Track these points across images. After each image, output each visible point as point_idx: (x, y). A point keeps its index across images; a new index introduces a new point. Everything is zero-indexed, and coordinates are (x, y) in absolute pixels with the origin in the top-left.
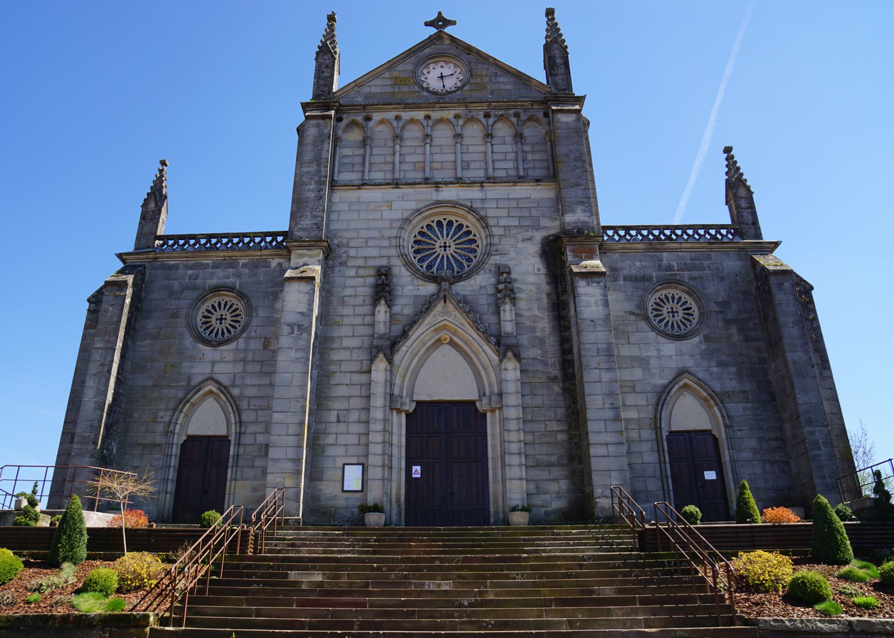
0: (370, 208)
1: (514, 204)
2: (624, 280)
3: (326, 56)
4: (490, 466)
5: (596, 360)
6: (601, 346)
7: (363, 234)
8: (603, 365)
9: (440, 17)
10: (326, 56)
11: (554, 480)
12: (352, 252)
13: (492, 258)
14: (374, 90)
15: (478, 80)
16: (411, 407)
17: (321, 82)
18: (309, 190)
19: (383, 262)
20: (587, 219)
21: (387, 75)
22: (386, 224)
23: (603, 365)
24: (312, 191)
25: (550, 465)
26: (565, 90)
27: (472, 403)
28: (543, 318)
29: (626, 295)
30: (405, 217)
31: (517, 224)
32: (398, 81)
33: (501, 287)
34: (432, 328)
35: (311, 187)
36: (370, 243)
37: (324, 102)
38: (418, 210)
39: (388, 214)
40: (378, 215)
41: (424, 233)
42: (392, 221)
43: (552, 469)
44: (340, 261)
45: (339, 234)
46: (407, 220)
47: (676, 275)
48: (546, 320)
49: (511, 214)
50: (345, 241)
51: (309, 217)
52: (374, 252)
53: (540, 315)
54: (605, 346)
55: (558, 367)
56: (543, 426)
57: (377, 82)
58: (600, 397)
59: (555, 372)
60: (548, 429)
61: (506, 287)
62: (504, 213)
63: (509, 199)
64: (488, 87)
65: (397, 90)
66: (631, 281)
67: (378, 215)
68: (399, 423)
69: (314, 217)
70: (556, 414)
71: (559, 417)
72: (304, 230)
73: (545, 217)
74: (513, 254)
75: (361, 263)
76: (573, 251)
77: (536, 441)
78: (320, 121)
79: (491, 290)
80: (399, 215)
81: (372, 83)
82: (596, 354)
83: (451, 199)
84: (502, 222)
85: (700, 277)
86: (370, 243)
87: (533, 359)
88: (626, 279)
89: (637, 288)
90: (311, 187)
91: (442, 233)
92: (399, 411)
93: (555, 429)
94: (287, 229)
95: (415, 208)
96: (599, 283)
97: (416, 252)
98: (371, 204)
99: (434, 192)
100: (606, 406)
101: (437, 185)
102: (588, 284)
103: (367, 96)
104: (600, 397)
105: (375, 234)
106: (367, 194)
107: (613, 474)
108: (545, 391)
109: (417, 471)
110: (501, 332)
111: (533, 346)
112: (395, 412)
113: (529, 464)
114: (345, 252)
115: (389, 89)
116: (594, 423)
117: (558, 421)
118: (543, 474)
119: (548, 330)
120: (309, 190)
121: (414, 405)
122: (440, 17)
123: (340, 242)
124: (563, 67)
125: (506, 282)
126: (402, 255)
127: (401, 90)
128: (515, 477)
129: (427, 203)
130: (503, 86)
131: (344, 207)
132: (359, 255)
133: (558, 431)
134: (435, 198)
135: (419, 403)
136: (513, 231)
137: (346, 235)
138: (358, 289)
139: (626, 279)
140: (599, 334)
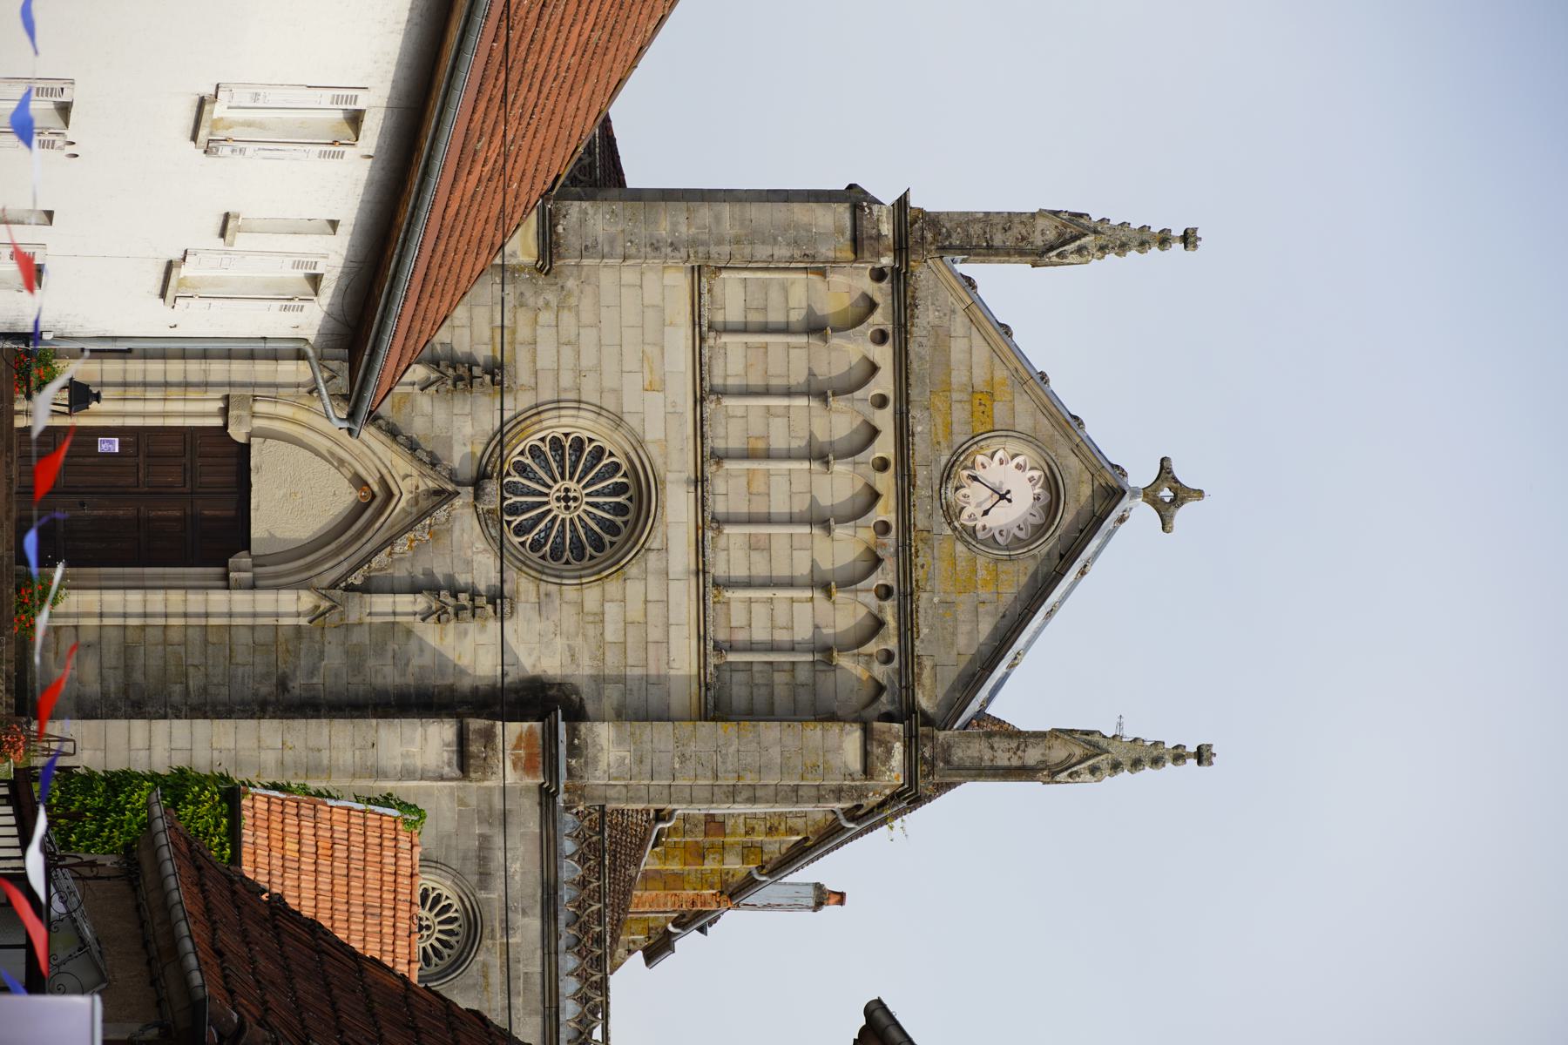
0: (648, 349)
1: (655, 634)
2: (481, 835)
3: (1062, 238)
4: (96, 570)
5: (299, 744)
6: (325, 755)
7: (589, 336)
8: (289, 756)
9: (1182, 494)
10: (1062, 238)
11: (101, 674)
12: (546, 317)
13: (532, 587)
14: (958, 348)
15: (982, 573)
16: (238, 433)
17: (975, 230)
18: (675, 225)
19: (524, 376)
20: (603, 765)
21: (1001, 373)
22: (609, 382)
23: (289, 756)
24: (674, 231)
25: (128, 669)
26: (947, 762)
27: (246, 544)
28: (403, 674)
29: (449, 836)
30: (626, 418)
31: (609, 637)
32: (982, 398)
33: (464, 598)
34: (384, 471)
35: (683, 229)
36: (567, 352)
37: (907, 245)
38: (641, 443)
39: (632, 385)
40: (631, 362)
41: (582, 450)
42: (617, 392)
43: (120, 672)
44: (528, 294)
45: (588, 289)
46: (618, 421)
47: (493, 938)
48: (398, 680)
49: (630, 628)
50: (573, 301)
51: (613, 230)
52: (546, 358)
53: (410, 669)
54: (325, 762)
55: (304, 694)
56: (196, 662)
57: (981, 352)
58: (232, 746)
59: (297, 685)
60: (191, 670)
61: (464, 608)
62: (635, 613)
63: (668, 625)
64: (963, 597)
65: (956, 396)
66: (481, 848)
67: (631, 362)
68: (199, 412)
69: (612, 241)
70: (218, 685)
71: (212, 690)
72: (582, 222)
73: (624, 695)
74: (538, 626)
75: (524, 333)
76: (531, 732)
77: (169, 648)
78: (848, 234)
79: (463, 579)
80: (630, 404)
81: (977, 340)
82: (310, 744)
83: (669, 510)
84: (612, 610)
85: (488, 985)
86: (567, 352)
87: (322, 652)
88: (485, 839)
89: (464, 859)
90: (683, 229)
91: (597, 493)
92: (225, 412)
93: (191, 684)
94: (630, 185)
95: (649, 437)
96: (449, 764)
97: (535, 452)
98: (656, 351)
99: (684, 476)
100: (216, 753)
101: (700, 481)
102: (448, 745)
103: (941, 337)
104: (232, 746)
105: (588, 360)
106: (680, 339)
107: (100, 754)
108: (260, 669)
109: (111, 445)
110: (773, 704)
111: (347, 653)
112: (221, 404)
113: (129, 633)
114: (547, 304)
115: (958, 377)
116: (187, 731)
117: (205, 689)
118: (111, 658)
119: (379, 681)
120: (675, 225)
121: (242, 439)
122: (1182, 494)
123: (570, 294)
124: (1015, 762)
125: (474, 608)
126: (537, 410)
127: (956, 406)
128: (89, 606)
129: (658, 462)
130: (964, 628)
131: (652, 292)
132: (540, 331)
133: (187, 687)
134: (670, 477)
135: (245, 449)
136: (591, 631)
137: (587, 304)
138: (467, 332)
139: (485, 839)
140: (349, 755)
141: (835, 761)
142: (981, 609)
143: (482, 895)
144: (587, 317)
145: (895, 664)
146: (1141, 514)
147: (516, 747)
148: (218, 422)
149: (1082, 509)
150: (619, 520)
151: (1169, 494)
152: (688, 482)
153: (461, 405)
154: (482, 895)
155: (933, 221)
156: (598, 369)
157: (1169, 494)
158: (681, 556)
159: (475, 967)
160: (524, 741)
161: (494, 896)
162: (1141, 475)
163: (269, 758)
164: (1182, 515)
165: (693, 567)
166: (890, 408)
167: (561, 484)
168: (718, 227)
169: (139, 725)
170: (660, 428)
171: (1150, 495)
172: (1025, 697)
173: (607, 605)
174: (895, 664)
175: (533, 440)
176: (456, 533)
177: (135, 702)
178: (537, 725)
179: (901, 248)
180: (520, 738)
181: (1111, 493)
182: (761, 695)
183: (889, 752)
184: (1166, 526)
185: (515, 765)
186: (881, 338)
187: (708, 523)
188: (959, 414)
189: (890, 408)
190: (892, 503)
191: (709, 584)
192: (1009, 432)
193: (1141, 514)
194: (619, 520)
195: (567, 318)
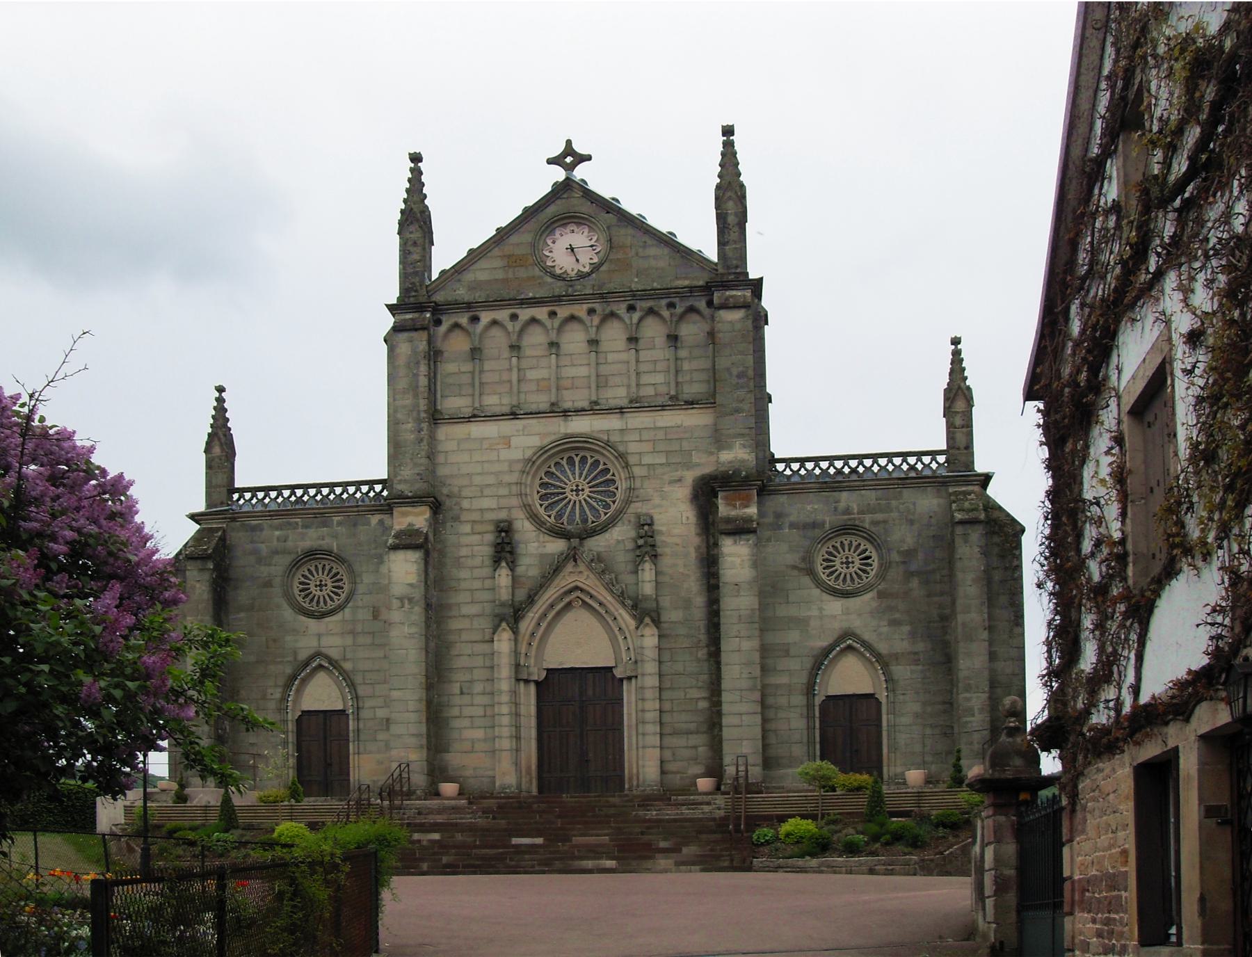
0: (485, 446)
1: (661, 435)
3: (415, 222)
6: (742, 613)
7: (478, 480)
9: (569, 149)
10: (415, 222)
14: (483, 277)
15: (620, 256)
19: (503, 515)
22: (505, 467)
27: (610, 669)
31: (664, 461)
32: (513, 261)
36: (486, 492)
39: (505, 454)
41: (547, 484)
42: (511, 462)
57: (483, 264)
62: (646, 447)
65: (510, 275)
66: (798, 528)
68: (529, 697)
71: (700, 684)
75: (476, 516)
76: (726, 498)
84: (647, 460)
92: (527, 681)
95: (538, 444)
99: (562, 423)
101: (565, 413)
103: (473, 287)
105: (491, 480)
112: (522, 684)
115: (500, 275)
122: (569, 149)
135: (548, 670)
136: (659, 471)
141: (738, 326)
142: (641, 254)
143: (827, 526)
144: (465, 482)
145: (676, 300)
146: (580, 173)
147: (735, 506)
148: (532, 688)
149: (569, 203)
150: (577, 460)
151: (570, 157)
152: (566, 421)
153: (521, 549)
154: (827, 526)
155: (405, 290)
156: (497, 474)
157: (570, 157)
158: (611, 423)
159: (873, 529)
160: (730, 503)
161: (827, 519)
162: (559, 174)
163: (747, 645)
164: (579, 148)
165: (618, 416)
166: (518, 311)
167: (569, 494)
168: (421, 410)
169: (725, 721)
170: (528, 438)
171: (570, 168)
172: (701, 237)
173: (502, 458)
174: (676, 300)
175: (542, 510)
176: (600, 549)
177: (713, 723)
178: (720, 495)
179: (420, 308)
180: (728, 504)
181: (563, 189)
182: (704, 376)
183: (732, 297)
184: (569, 142)
185: (747, 507)
186: (475, 319)
187: (594, 408)
188: (522, 273)
189: (518, 311)
190: (577, 307)
191: (637, 404)
192: (533, 245)
193: (580, 173)
194: (577, 460)
195: (465, 493)
